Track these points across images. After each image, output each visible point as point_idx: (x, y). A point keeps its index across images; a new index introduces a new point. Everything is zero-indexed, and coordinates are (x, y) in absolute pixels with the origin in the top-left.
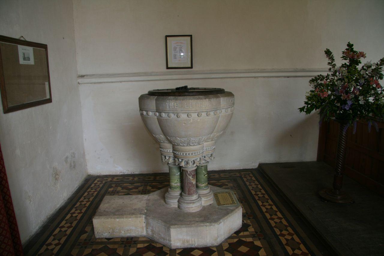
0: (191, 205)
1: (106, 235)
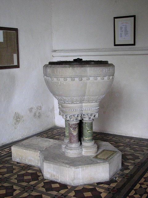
0: (69, 151)
1: (18, 160)
